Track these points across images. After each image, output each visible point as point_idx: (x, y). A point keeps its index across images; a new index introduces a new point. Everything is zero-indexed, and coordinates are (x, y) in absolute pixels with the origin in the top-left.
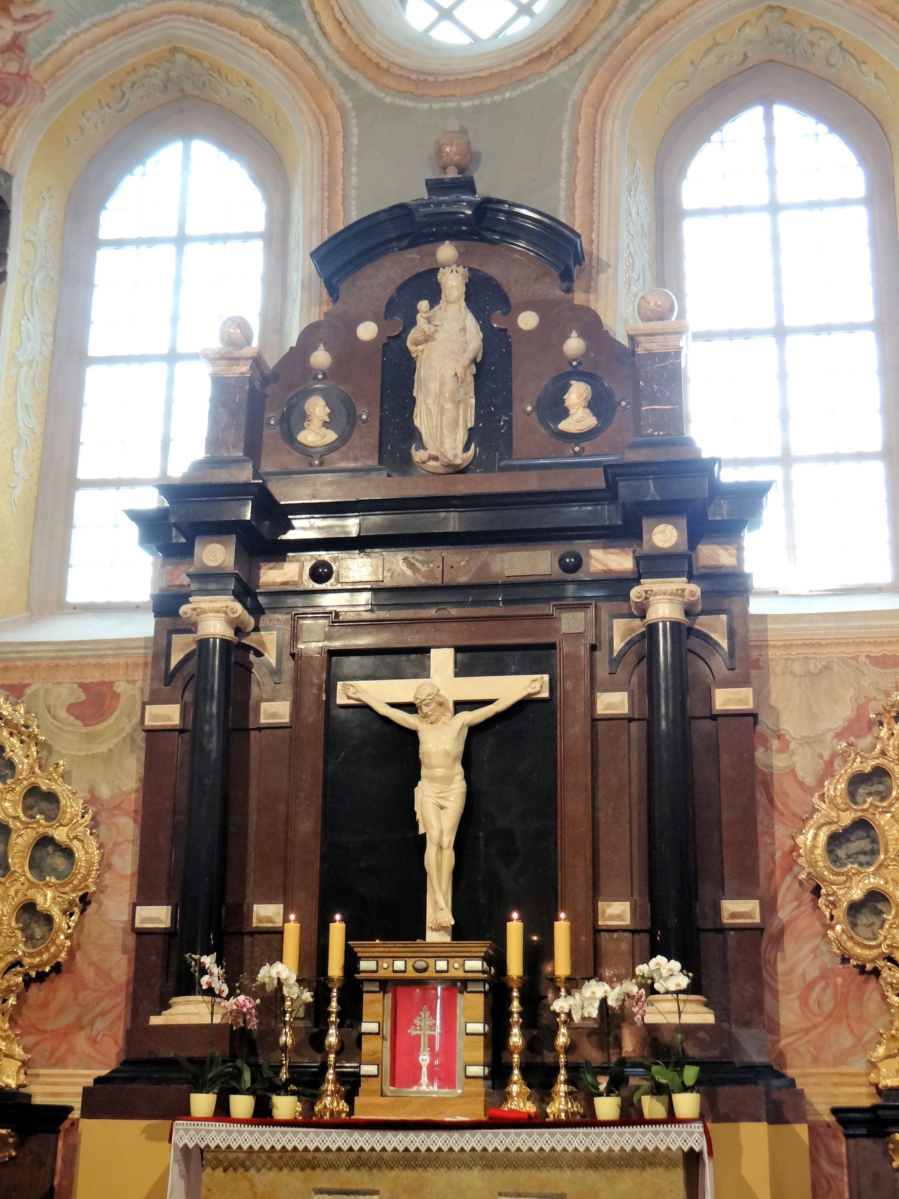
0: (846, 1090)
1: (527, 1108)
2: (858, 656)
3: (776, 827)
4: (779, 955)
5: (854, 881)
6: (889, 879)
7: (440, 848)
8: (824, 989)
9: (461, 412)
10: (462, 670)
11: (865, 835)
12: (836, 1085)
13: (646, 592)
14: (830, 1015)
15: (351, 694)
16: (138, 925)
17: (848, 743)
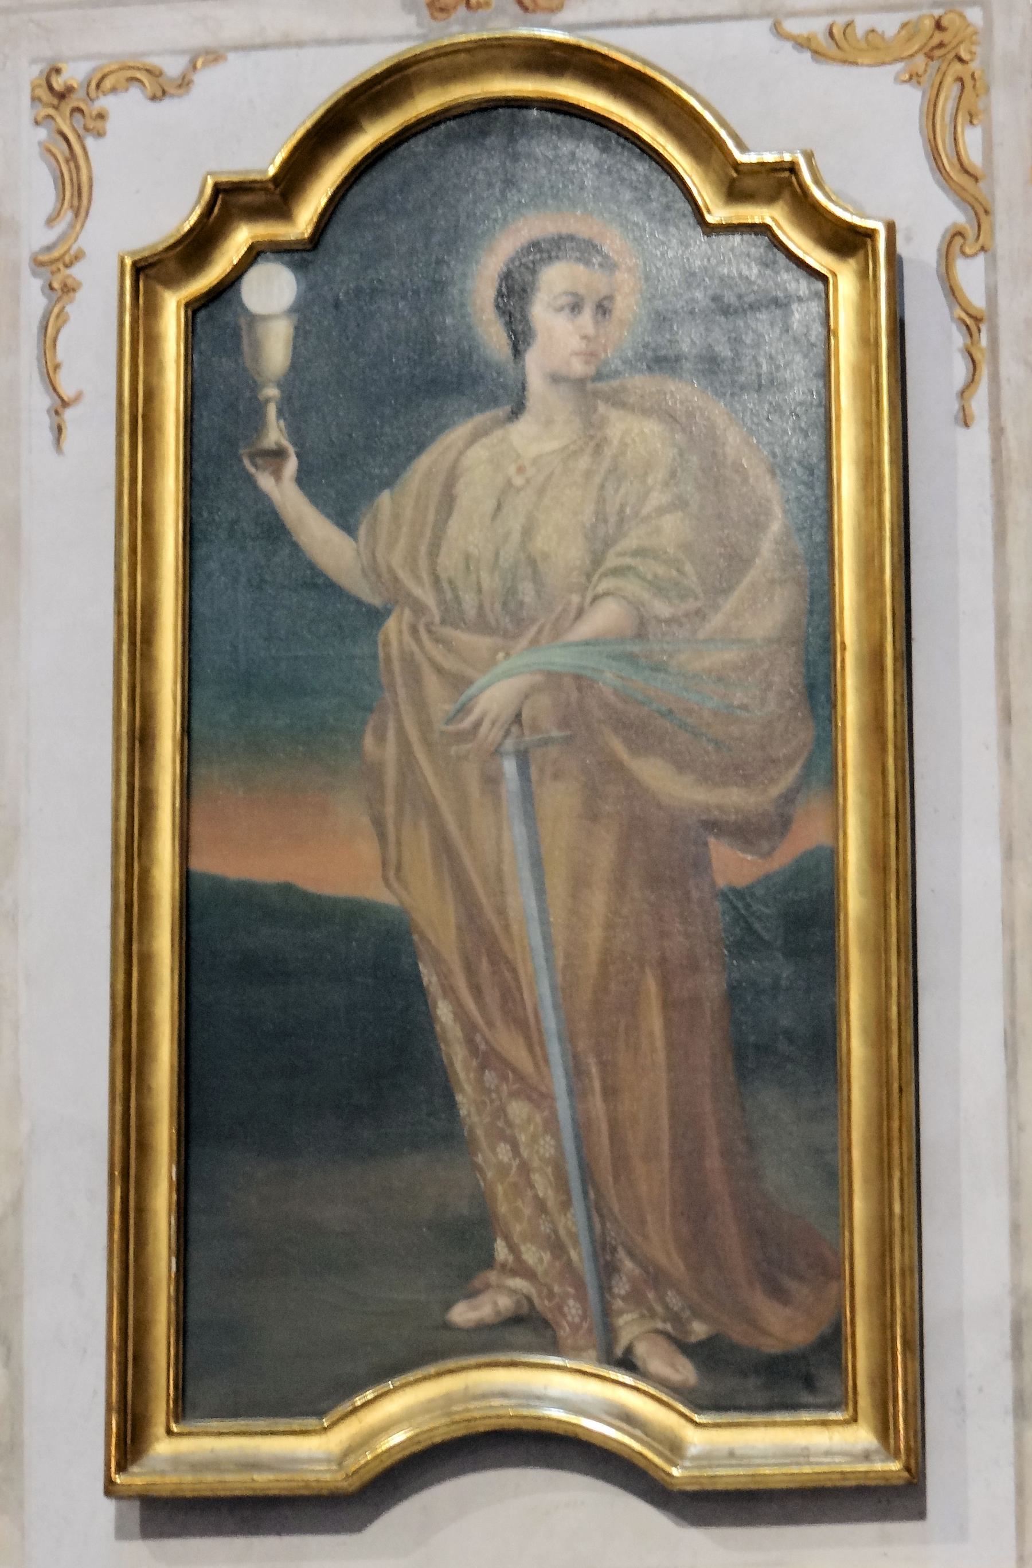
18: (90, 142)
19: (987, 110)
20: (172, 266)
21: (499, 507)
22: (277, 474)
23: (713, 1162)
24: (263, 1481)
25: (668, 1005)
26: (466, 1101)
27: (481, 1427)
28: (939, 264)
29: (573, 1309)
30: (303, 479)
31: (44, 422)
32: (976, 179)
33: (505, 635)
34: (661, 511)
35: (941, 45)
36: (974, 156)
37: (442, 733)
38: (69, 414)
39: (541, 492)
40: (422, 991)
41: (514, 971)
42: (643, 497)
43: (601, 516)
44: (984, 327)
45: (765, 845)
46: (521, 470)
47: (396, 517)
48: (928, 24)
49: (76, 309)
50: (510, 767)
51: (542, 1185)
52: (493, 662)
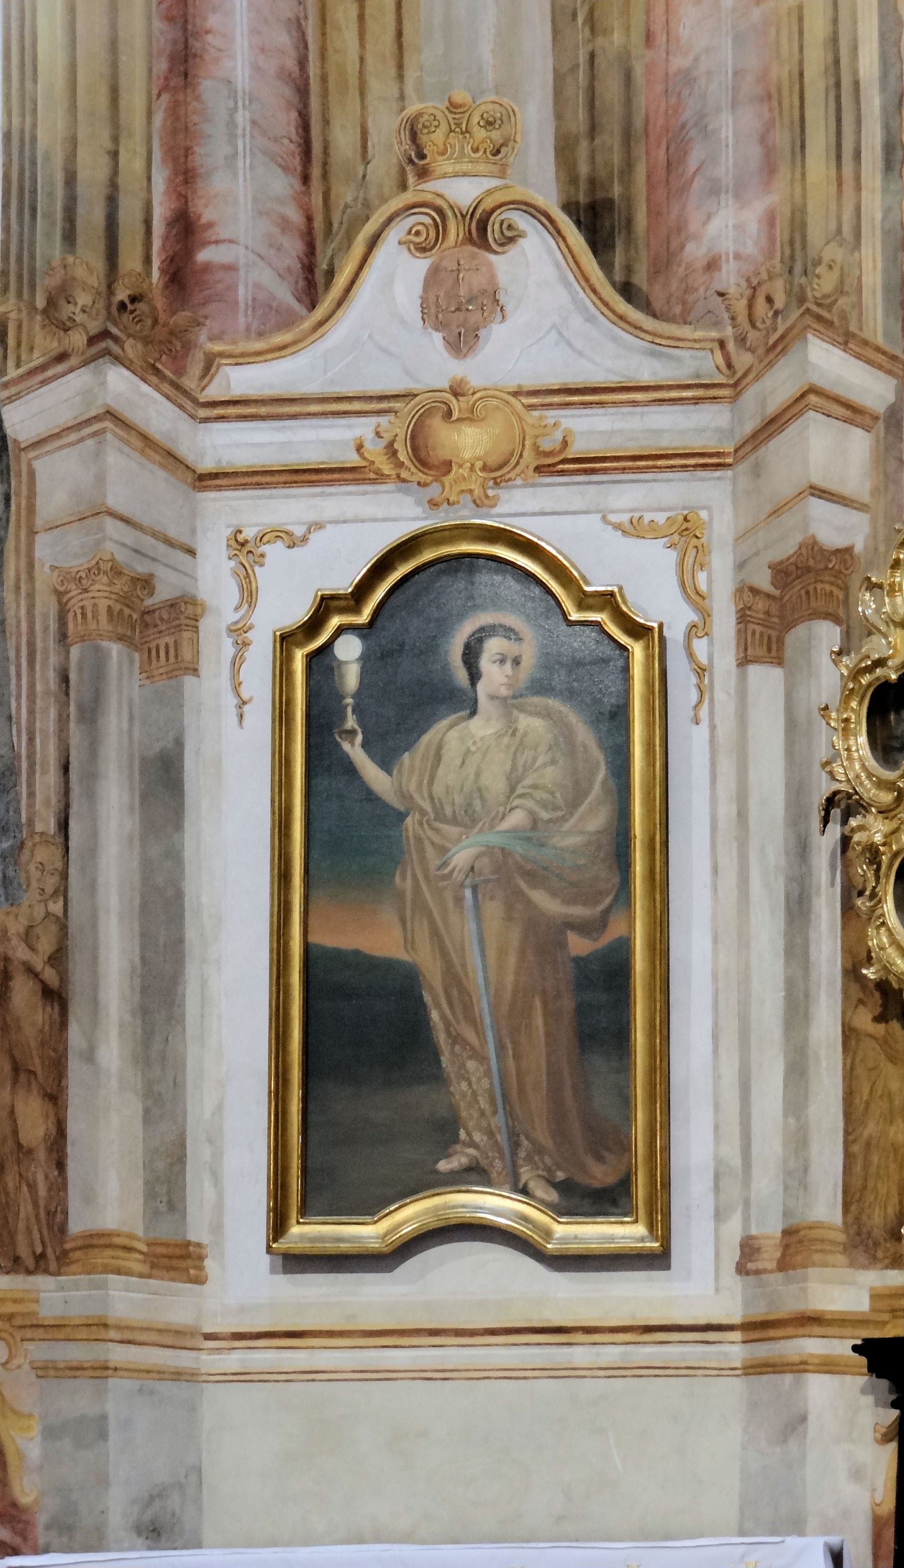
18: (257, 568)
19: (710, 563)
20: (300, 636)
21: (463, 763)
22: (352, 743)
23: (568, 1093)
24: (344, 1247)
25: (546, 1015)
26: (445, 1060)
27: (453, 1222)
28: (684, 641)
29: (498, 1163)
30: (364, 745)
31: (234, 712)
32: (704, 598)
33: (465, 826)
34: (545, 765)
35: (687, 529)
36: (703, 587)
37: (435, 876)
38: (246, 708)
39: (485, 754)
40: (423, 1005)
41: (470, 997)
42: (535, 759)
43: (514, 768)
44: (706, 674)
45: (595, 935)
46: (474, 743)
47: (412, 766)
48: (681, 518)
49: (250, 654)
50: (468, 893)
51: (483, 1103)
52: (459, 840)
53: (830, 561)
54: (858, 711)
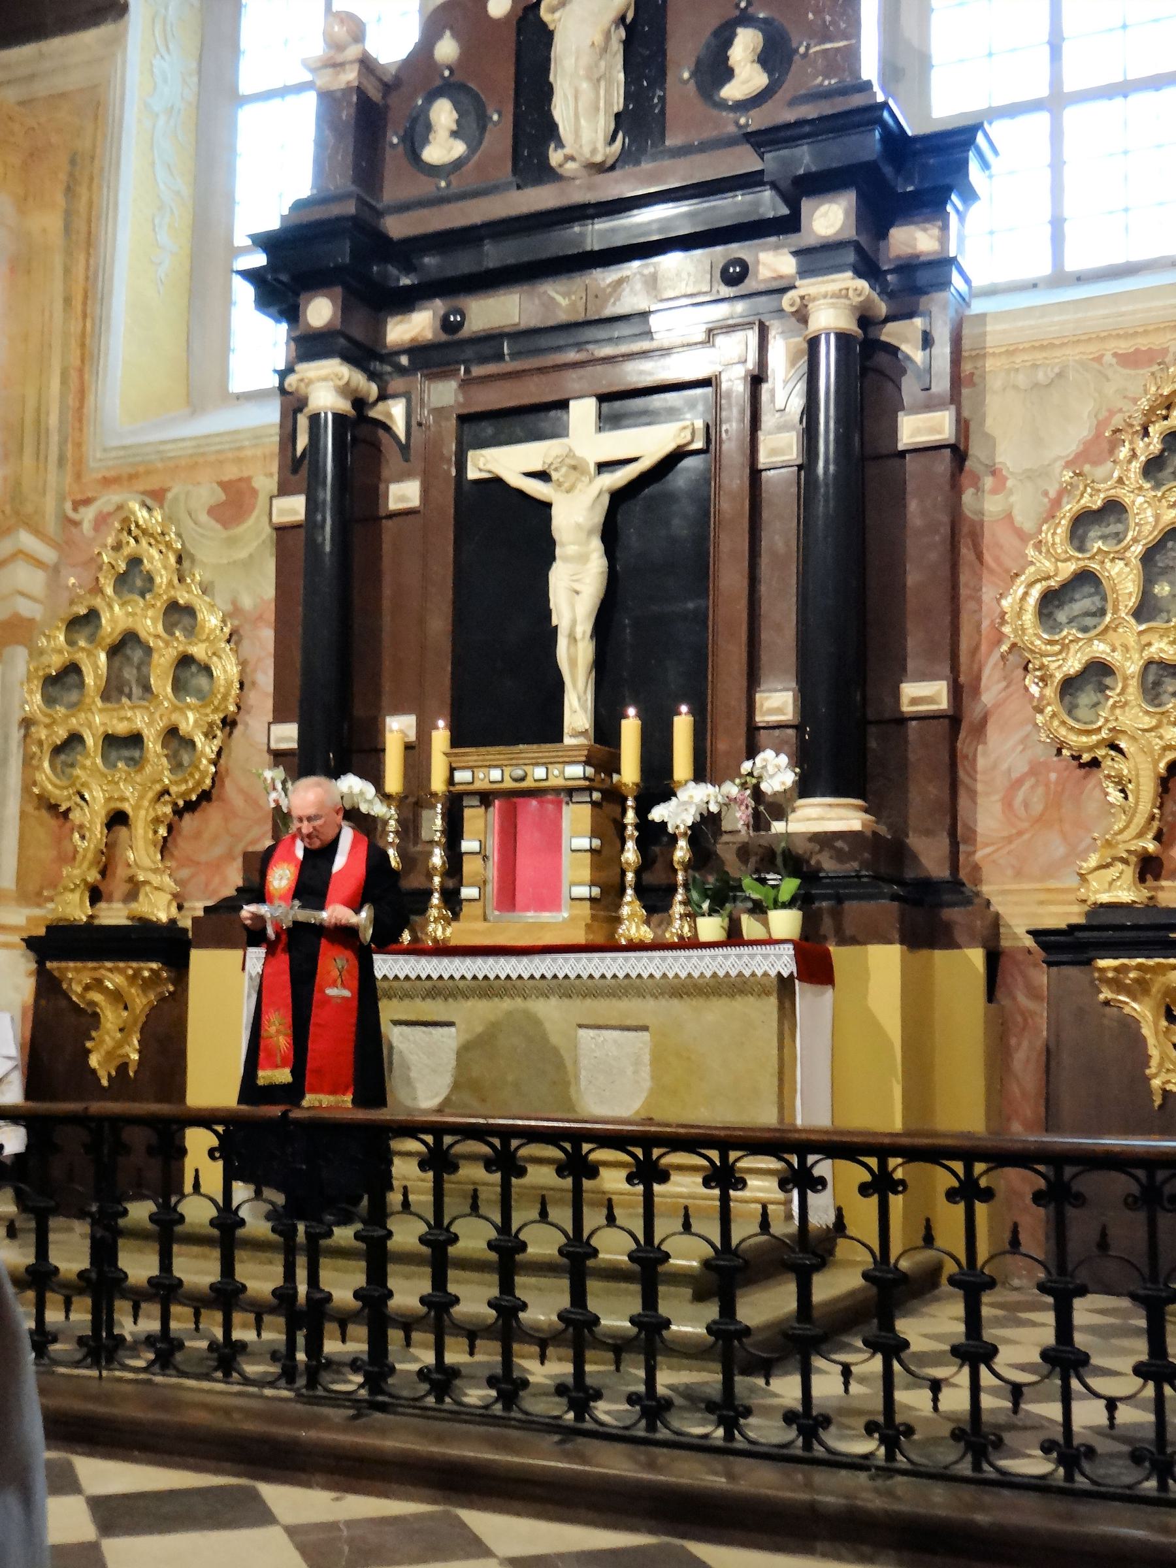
0: (1054, 909)
1: (642, 933)
2: (1102, 356)
3: (984, 590)
4: (980, 748)
5: (1072, 651)
6: (1117, 645)
7: (573, 638)
8: (1033, 787)
9: (602, 92)
10: (608, 421)
11: (1093, 590)
12: (1041, 903)
13: (802, 298)
14: (1039, 819)
15: (481, 466)
16: (273, 746)
17: (1074, 472)
53: (1136, 980)
54: (36, 685)
